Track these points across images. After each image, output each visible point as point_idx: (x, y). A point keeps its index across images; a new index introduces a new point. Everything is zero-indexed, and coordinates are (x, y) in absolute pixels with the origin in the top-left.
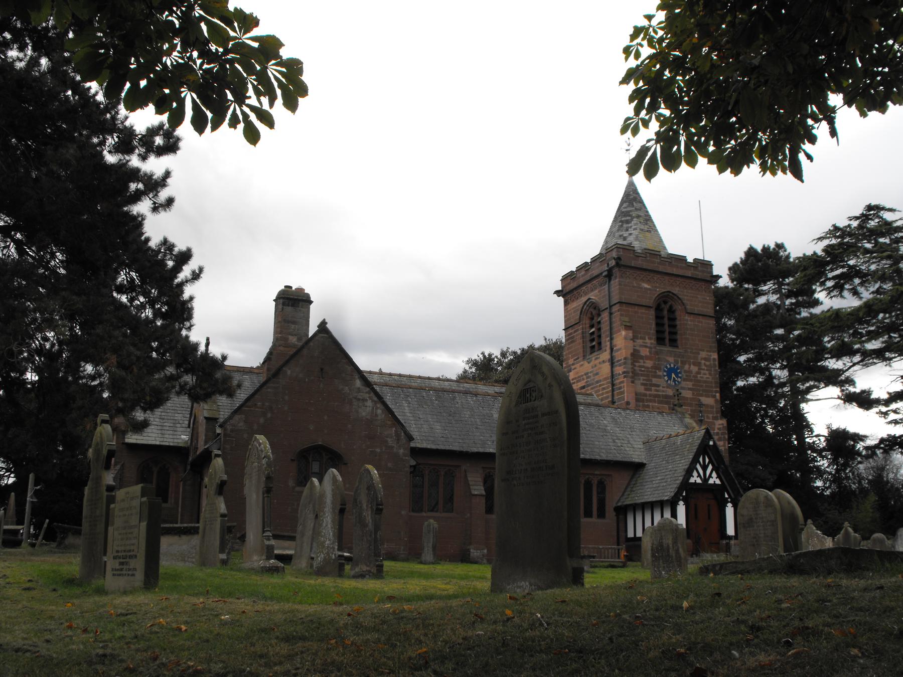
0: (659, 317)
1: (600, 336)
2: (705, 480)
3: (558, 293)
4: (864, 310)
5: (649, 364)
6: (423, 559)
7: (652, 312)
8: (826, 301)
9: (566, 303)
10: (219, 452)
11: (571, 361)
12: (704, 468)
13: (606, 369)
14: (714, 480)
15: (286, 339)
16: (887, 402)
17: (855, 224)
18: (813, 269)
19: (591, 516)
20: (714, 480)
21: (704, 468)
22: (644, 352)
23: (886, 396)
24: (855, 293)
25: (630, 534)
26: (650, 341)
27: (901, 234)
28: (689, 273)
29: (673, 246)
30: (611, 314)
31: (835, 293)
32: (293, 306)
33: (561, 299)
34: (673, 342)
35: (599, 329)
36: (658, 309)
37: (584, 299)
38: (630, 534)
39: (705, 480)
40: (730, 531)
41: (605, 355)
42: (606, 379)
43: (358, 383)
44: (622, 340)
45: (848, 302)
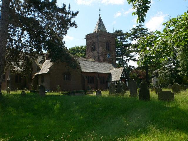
1: (95, 48)
2: (123, 77)
3: (85, 38)
4: (103, 30)
5: (105, 54)
8: (129, 41)
9: (87, 41)
10: (153, 61)
11: (88, 52)
14: (125, 77)
17: (137, 28)
18: (128, 35)
19: (102, 83)
20: (125, 77)
24: (135, 40)
26: (105, 49)
28: (111, 36)
29: (108, 32)
30: (98, 44)
31: (131, 40)
33: (86, 40)
34: (109, 50)
35: (95, 46)
37: (91, 40)
39: (123, 77)
40: (127, 86)
42: (96, 56)
44: (101, 49)
45: (134, 42)
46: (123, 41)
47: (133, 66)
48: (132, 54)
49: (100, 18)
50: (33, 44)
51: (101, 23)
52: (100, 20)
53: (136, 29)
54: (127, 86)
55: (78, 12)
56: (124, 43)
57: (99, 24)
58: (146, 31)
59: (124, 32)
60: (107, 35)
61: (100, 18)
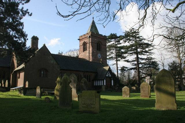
0: (97, 45)
2: (109, 76)
6: (96, 98)
7: (96, 44)
12: (109, 74)
13: (88, 54)
14: (110, 76)
15: (33, 46)
16: (131, 62)
18: (121, 38)
20: (110, 76)
21: (109, 74)
22: (95, 52)
23: (131, 61)
24: (128, 42)
25: (95, 85)
27: (184, 37)
28: (103, 38)
29: (100, 33)
32: (35, 40)
34: (100, 50)
36: (97, 44)
38: (95, 85)
40: (112, 85)
41: (88, 52)
43: (51, 56)
45: (127, 44)
46: (118, 44)
47: (126, 66)
48: (125, 55)
49: (93, 21)
50: (178, 78)
51: (93, 26)
52: (93, 23)
53: (129, 33)
54: (112, 85)
55: (32, 13)
56: (119, 46)
57: (92, 26)
58: (138, 35)
59: (118, 35)
60: (98, 37)
61: (93, 21)
